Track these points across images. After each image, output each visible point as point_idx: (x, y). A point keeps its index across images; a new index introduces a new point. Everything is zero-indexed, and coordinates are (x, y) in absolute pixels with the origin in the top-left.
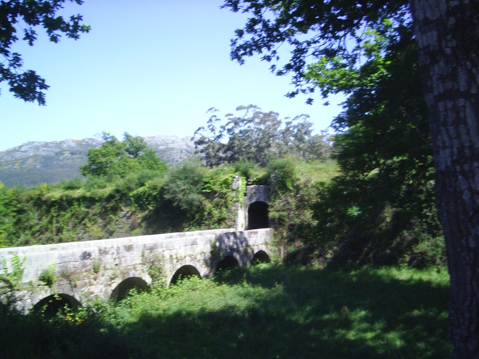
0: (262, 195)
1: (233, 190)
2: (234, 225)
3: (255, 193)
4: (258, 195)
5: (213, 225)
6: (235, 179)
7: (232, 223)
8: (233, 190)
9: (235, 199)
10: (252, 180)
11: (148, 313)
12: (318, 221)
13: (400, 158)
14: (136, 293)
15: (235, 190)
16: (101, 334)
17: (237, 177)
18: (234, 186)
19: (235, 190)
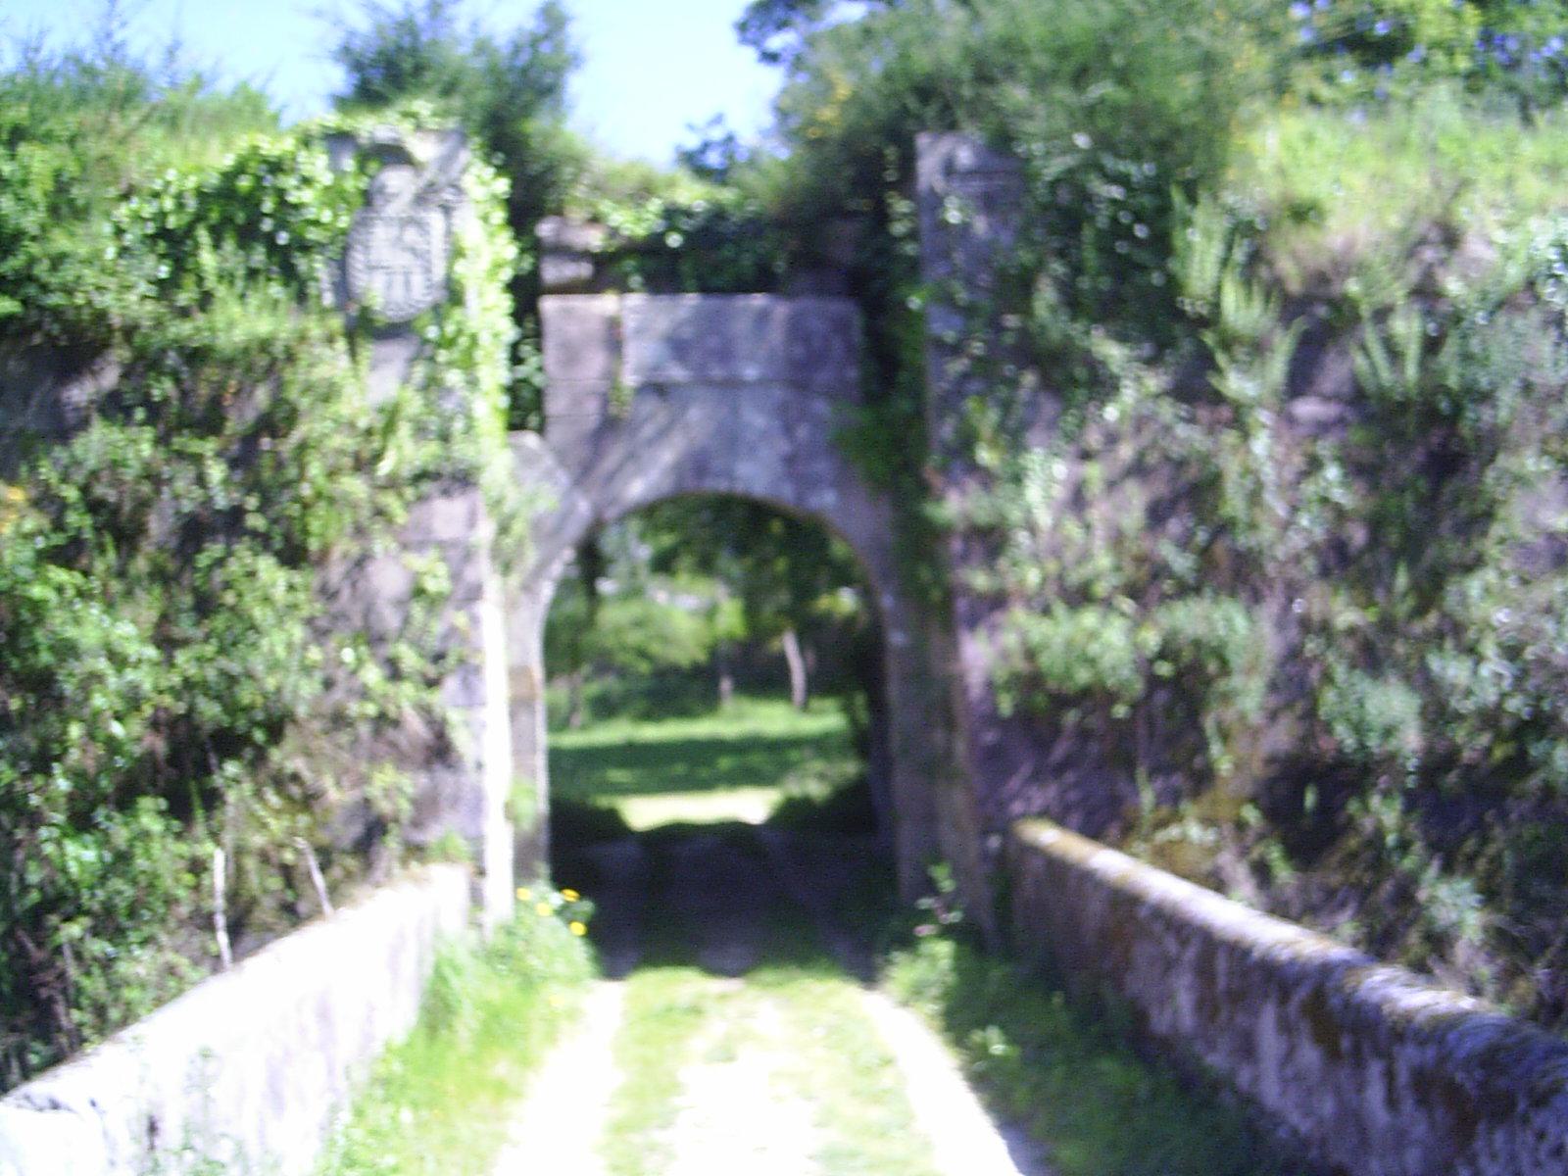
0: (756, 419)
1: (364, 328)
2: (426, 808)
3: (656, 388)
4: (699, 418)
5: (81, 822)
6: (397, 181)
7: (393, 786)
8: (364, 328)
9: (404, 453)
10: (595, 239)
11: (1485, 943)
12: (1349, 912)
13: (1108, 862)
14: (1030, 127)
15: (395, 331)
16: (1011, 1039)
17: (424, 149)
18: (389, 278)
19: (395, 331)
